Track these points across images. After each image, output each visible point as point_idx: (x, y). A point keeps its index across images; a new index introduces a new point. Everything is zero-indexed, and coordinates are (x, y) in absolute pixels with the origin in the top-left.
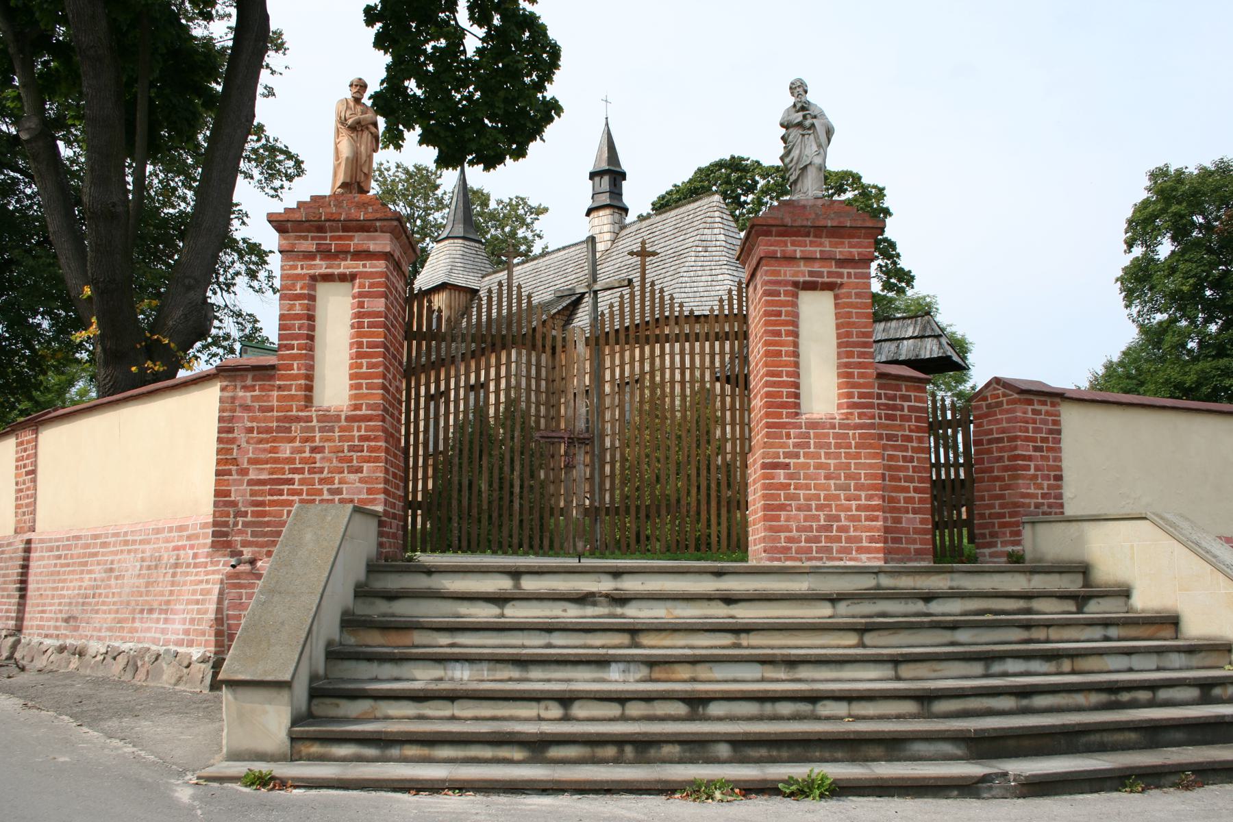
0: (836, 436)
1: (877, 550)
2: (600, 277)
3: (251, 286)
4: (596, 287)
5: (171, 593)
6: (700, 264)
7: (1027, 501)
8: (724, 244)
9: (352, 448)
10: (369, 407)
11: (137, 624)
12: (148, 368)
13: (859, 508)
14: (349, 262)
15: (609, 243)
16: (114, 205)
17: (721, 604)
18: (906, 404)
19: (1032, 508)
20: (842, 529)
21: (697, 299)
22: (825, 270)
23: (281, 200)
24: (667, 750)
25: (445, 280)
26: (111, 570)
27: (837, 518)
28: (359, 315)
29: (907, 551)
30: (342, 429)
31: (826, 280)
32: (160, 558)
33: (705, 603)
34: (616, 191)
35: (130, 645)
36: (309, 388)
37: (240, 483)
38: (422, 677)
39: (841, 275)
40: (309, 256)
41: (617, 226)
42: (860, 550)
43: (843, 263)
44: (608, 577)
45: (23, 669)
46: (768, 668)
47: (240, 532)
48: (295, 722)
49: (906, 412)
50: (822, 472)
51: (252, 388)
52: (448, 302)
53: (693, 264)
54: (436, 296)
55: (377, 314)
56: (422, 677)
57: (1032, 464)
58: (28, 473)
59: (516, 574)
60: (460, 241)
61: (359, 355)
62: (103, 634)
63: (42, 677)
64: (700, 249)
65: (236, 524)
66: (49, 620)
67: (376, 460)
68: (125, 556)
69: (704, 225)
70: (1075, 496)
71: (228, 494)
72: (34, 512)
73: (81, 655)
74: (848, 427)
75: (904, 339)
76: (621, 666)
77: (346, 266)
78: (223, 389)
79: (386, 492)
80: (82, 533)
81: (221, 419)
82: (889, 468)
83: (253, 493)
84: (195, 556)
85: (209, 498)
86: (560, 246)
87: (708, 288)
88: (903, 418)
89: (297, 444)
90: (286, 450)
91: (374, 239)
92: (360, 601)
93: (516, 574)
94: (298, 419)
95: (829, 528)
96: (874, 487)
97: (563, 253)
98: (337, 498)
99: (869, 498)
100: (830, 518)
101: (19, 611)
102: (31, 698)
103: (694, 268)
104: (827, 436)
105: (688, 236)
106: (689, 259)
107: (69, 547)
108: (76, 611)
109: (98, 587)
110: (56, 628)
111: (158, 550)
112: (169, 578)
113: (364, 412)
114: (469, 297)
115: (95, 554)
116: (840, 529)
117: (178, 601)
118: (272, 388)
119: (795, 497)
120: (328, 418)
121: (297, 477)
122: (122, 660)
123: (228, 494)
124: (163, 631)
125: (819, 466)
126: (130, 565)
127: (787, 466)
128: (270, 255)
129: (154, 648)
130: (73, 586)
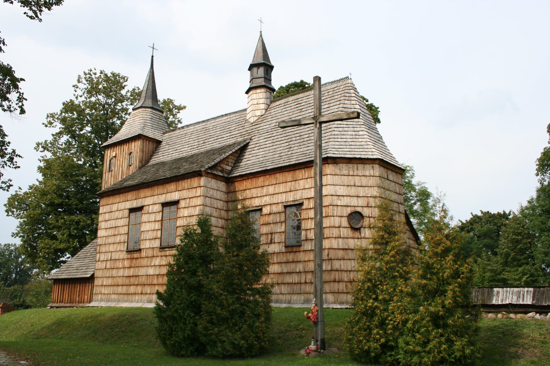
2: (324, 112)
15: (264, 111)
25: (141, 132)
34: (268, 78)
41: (268, 100)
52: (141, 148)
54: (133, 144)
60: (150, 110)
69: (345, 98)
86: (224, 114)
87: (355, 140)
97: (226, 118)
103: (342, 126)
105: (332, 105)
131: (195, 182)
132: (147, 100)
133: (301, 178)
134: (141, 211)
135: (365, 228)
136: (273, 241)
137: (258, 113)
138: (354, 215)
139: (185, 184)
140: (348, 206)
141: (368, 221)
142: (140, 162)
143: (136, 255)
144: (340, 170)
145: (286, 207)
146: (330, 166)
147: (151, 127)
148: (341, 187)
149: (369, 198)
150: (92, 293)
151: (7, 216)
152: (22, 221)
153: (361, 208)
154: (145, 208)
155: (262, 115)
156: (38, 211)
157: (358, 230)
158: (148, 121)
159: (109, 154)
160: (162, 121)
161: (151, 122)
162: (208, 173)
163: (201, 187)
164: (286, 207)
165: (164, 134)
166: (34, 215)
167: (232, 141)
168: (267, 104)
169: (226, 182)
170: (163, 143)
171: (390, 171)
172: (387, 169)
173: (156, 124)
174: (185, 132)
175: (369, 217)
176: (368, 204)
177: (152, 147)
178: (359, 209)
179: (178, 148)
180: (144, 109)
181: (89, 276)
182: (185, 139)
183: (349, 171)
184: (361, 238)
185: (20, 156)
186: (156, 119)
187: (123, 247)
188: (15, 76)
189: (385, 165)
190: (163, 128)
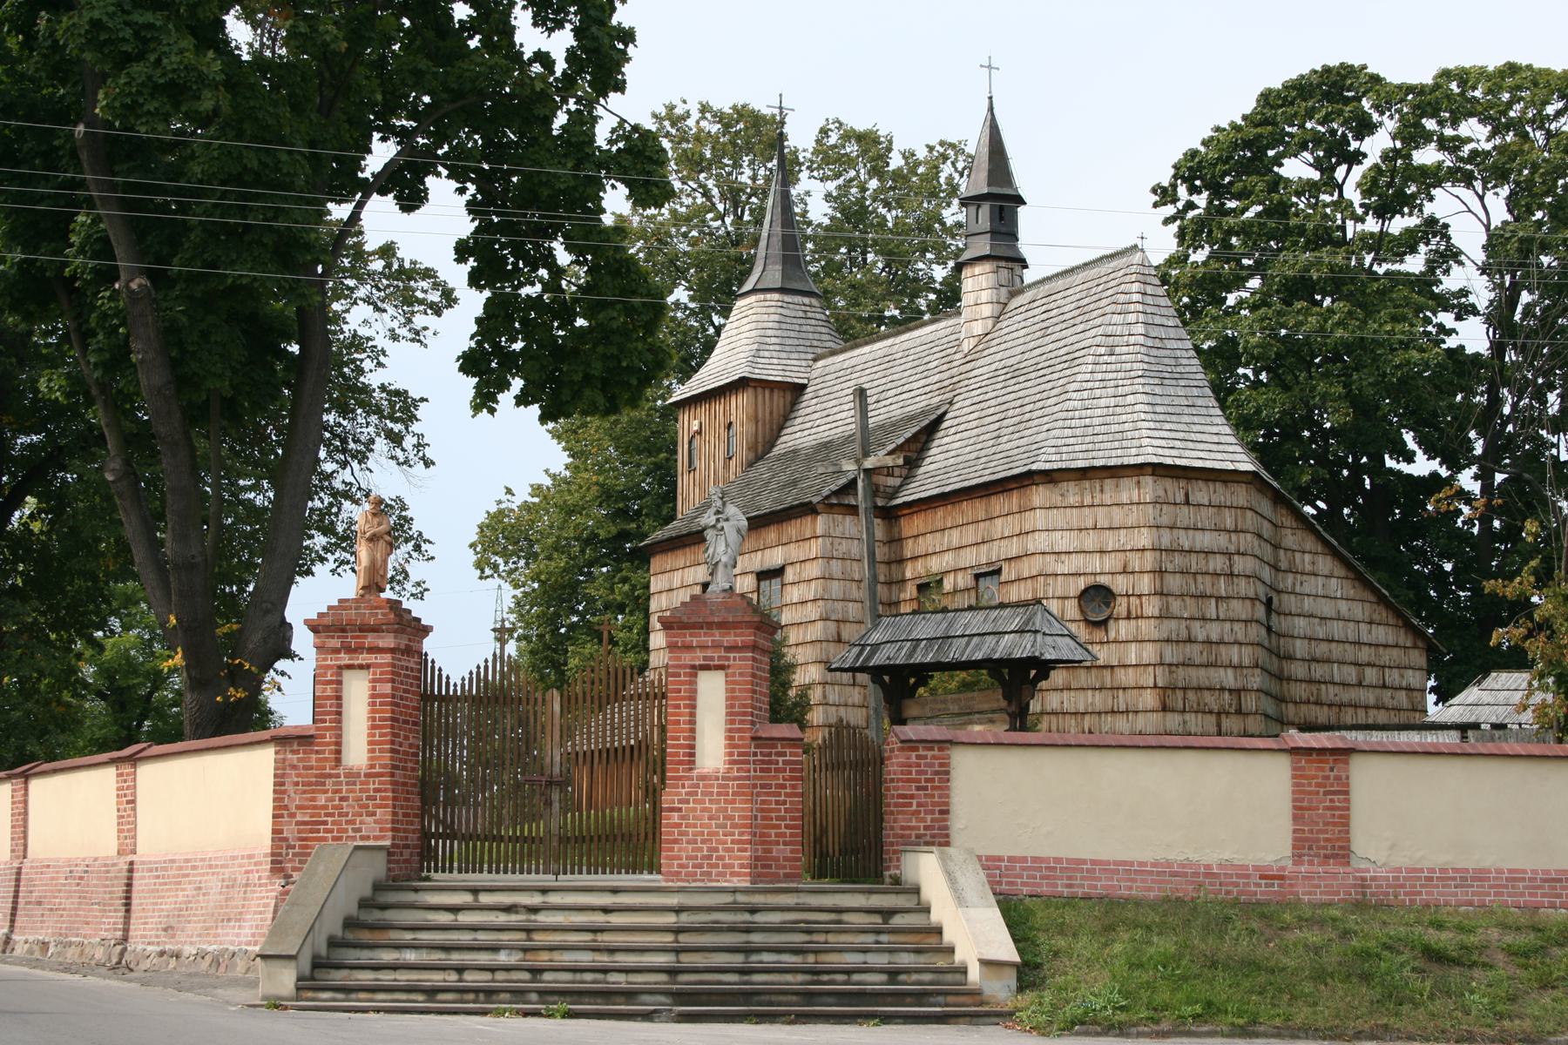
0: (719, 786)
1: (745, 874)
3: (392, 458)
5: (243, 906)
6: (1100, 376)
7: (907, 832)
8: (1141, 339)
9: (368, 798)
10: (381, 766)
11: (219, 931)
12: (231, 696)
13: (733, 842)
14: (365, 655)
15: (990, 323)
16: (193, 557)
17: (601, 914)
18: (781, 759)
19: (913, 839)
20: (721, 858)
21: (1088, 439)
22: (716, 655)
23: (426, 346)
24: (503, 996)
26: (200, 888)
27: (716, 850)
28: (373, 696)
29: (777, 875)
30: (362, 783)
31: (716, 663)
32: (235, 880)
33: (590, 913)
35: (215, 947)
36: (339, 752)
37: (290, 823)
38: (388, 956)
39: (728, 659)
40: (337, 651)
42: (733, 874)
43: (729, 649)
44: (538, 894)
45: (131, 970)
46: (597, 953)
47: (291, 861)
48: (299, 979)
49: (781, 765)
50: (706, 814)
51: (297, 752)
52: (751, 411)
53: (1088, 376)
55: (386, 696)
56: (388, 956)
57: (914, 802)
58: (128, 802)
59: (475, 891)
60: (776, 296)
61: (373, 727)
62: (194, 939)
63: (148, 974)
64: (1102, 350)
65: (287, 854)
66: (152, 929)
67: (386, 806)
68: (210, 877)
70: (966, 828)
71: (281, 832)
72: (134, 837)
73: (177, 957)
74: (728, 779)
75: (1006, 633)
76: (507, 951)
77: (363, 658)
78: (276, 753)
79: (393, 829)
80: (177, 857)
81: (276, 776)
82: (762, 810)
83: (299, 832)
84: (260, 878)
85: (268, 834)
87: (1108, 419)
88: (777, 770)
89: (330, 795)
90: (322, 800)
91: (382, 638)
92: (362, 910)
93: (475, 891)
94: (330, 776)
95: (710, 857)
96: (744, 826)
98: (358, 835)
99: (741, 834)
100: (710, 849)
101: (125, 923)
102: (144, 983)
103: (1090, 385)
104: (712, 786)
106: (1083, 368)
107: (165, 869)
108: (173, 922)
109: (190, 902)
110: (157, 936)
111: (234, 873)
112: (241, 895)
113: (377, 770)
114: (789, 397)
115: (187, 875)
116: (719, 858)
117: (247, 912)
118: (312, 752)
119: (686, 834)
120: (352, 775)
121: (330, 819)
122: (208, 959)
123: (281, 832)
124: (238, 935)
125: (703, 810)
126: (214, 884)
127: (680, 810)
128: (422, 405)
129: (231, 948)
130: (169, 903)
131: (805, 526)
132: (769, 267)
133: (997, 514)
138: (1092, 592)
139: (793, 529)
141: (1125, 605)
142: (749, 449)
144: (1062, 495)
145: (977, 577)
146: (1041, 488)
147: (777, 348)
151: (481, 578)
152: (520, 595)
156: (562, 562)
157: (1103, 624)
158: (770, 332)
159: (689, 423)
160: (813, 322)
161: (779, 333)
162: (832, 506)
163: (817, 537)
164: (977, 577)
165: (815, 360)
166: (550, 574)
168: (998, 303)
169: (883, 519)
170: (809, 390)
173: (792, 334)
175: (1128, 595)
176: (1125, 567)
177: (781, 404)
178: (1103, 580)
180: (762, 297)
183: (1082, 495)
184: (1108, 642)
185: (430, 542)
186: (794, 321)
190: (815, 343)
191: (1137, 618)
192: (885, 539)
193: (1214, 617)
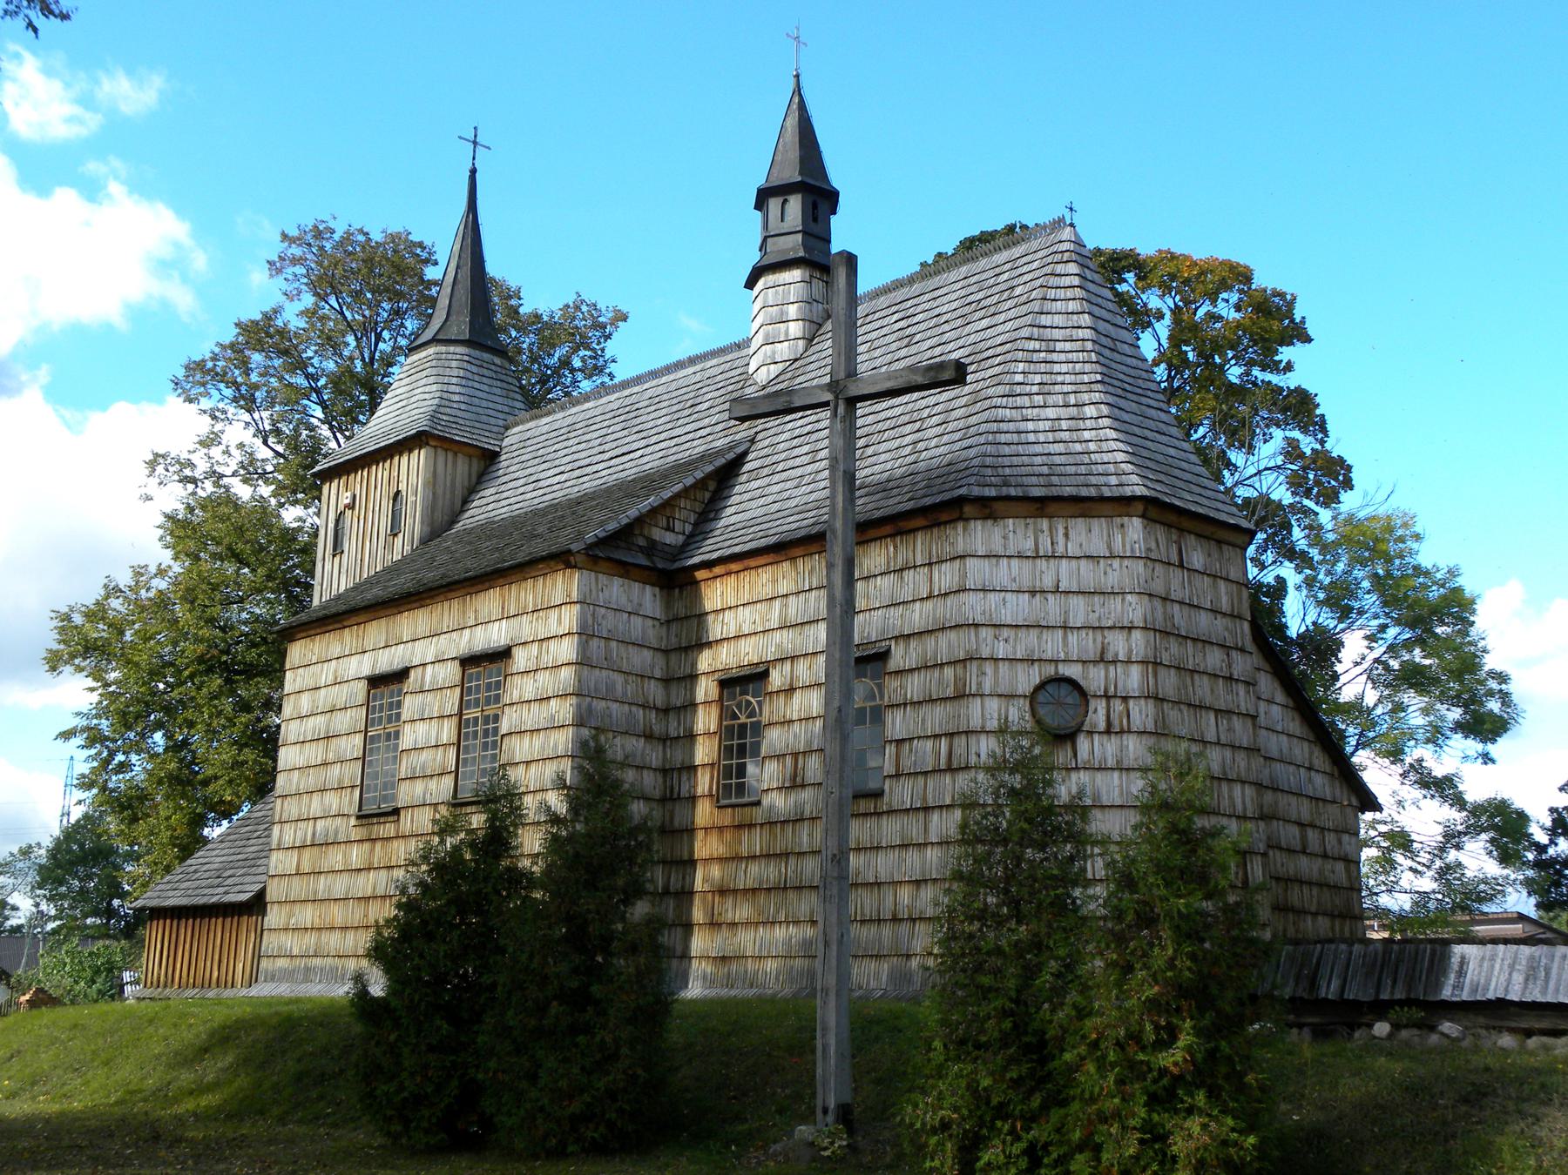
4: (854, 390)
6: (1038, 378)
15: (801, 343)
54: (405, 459)
97: (691, 370)
134: (401, 681)
135: (1090, 733)
136: (799, 780)
137: (784, 351)
140: (1033, 661)
141: (1102, 712)
143: (388, 829)
147: (463, 407)
148: (1009, 595)
149: (1106, 632)
150: (258, 956)
153: (1080, 666)
154: (412, 673)
155: (796, 360)
158: (453, 388)
167: (699, 448)
169: (662, 588)
171: (1193, 537)
172: (1181, 530)
174: (569, 421)
176: (1103, 653)
177: (466, 473)
179: (542, 476)
180: (443, 349)
181: (244, 897)
182: (566, 444)
187: (348, 802)
188: (180, 212)
189: (1172, 518)
191: (1122, 732)
192: (664, 618)
193: (1214, 739)
